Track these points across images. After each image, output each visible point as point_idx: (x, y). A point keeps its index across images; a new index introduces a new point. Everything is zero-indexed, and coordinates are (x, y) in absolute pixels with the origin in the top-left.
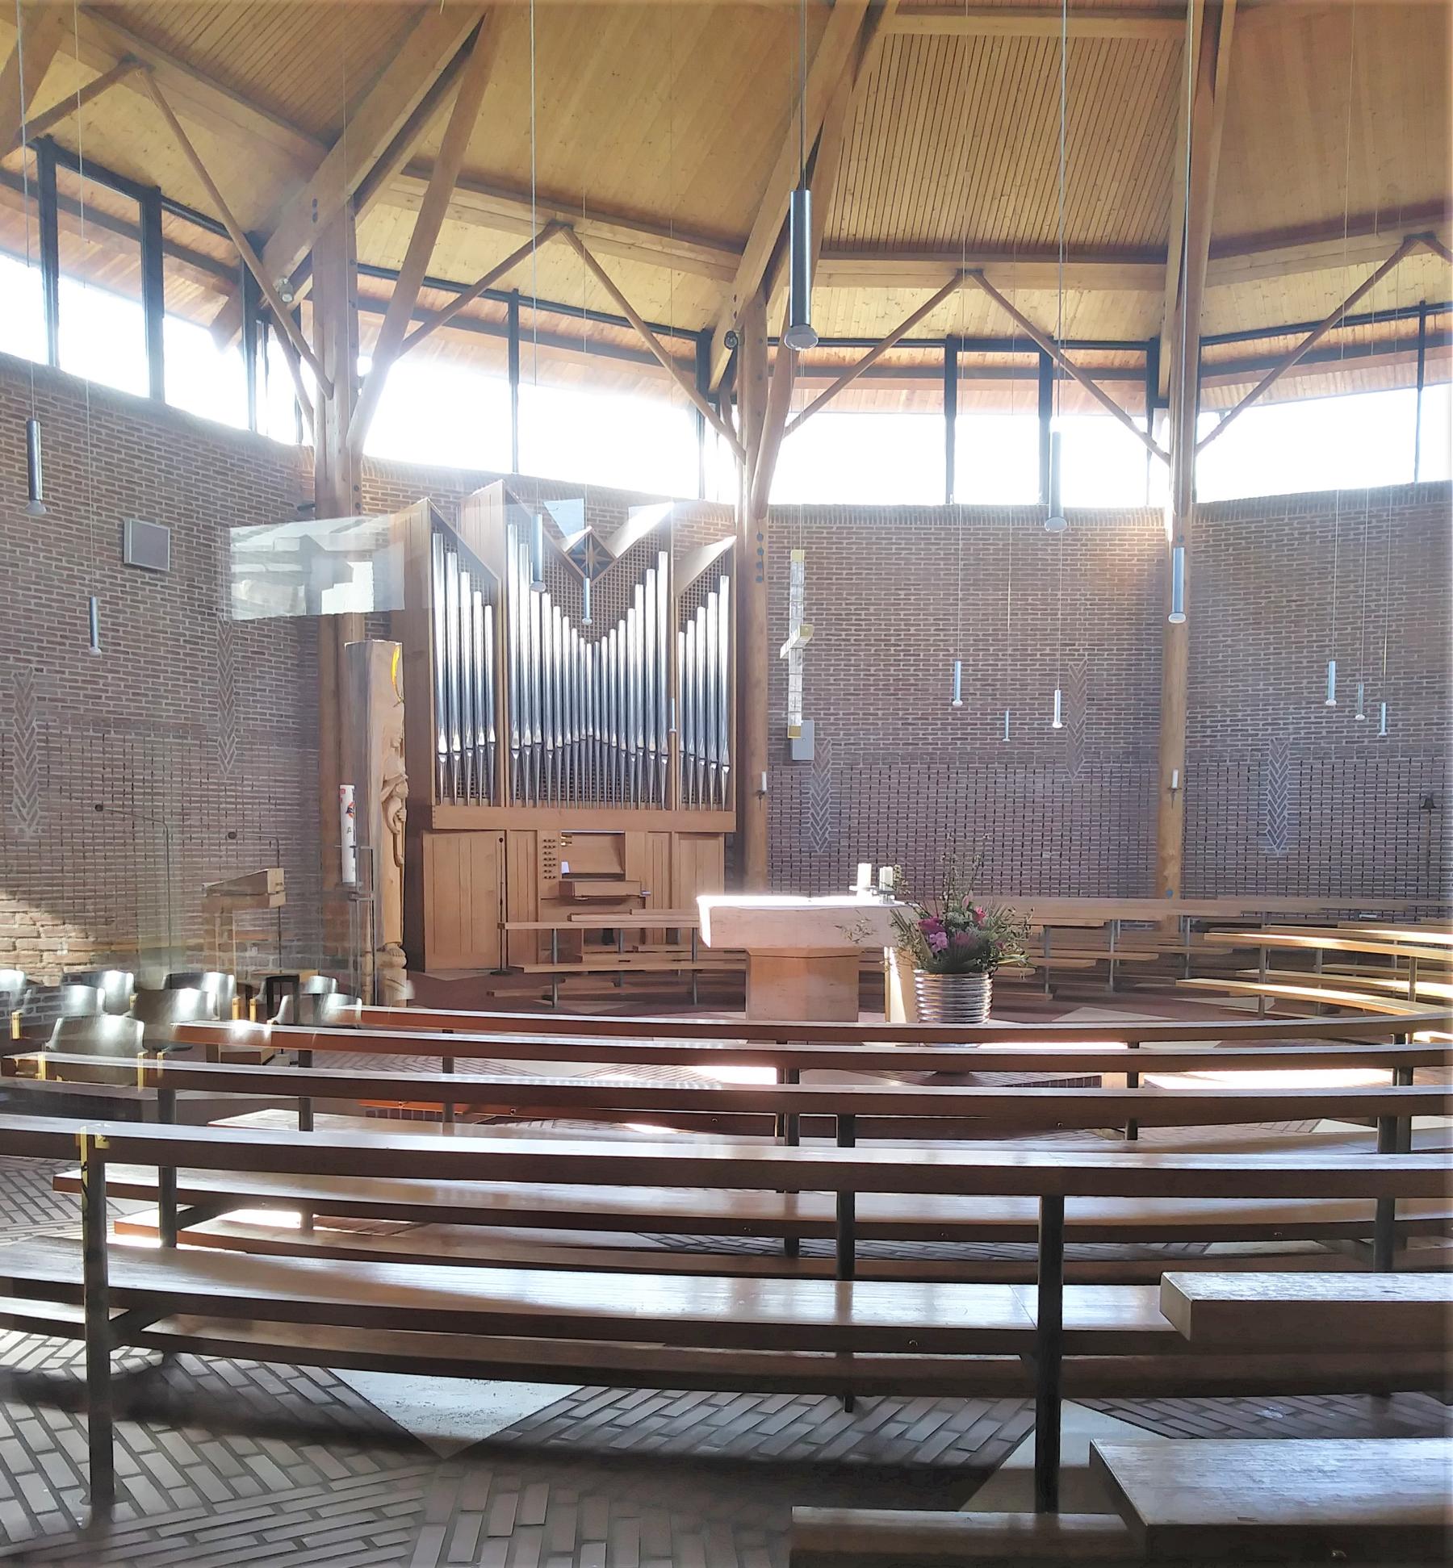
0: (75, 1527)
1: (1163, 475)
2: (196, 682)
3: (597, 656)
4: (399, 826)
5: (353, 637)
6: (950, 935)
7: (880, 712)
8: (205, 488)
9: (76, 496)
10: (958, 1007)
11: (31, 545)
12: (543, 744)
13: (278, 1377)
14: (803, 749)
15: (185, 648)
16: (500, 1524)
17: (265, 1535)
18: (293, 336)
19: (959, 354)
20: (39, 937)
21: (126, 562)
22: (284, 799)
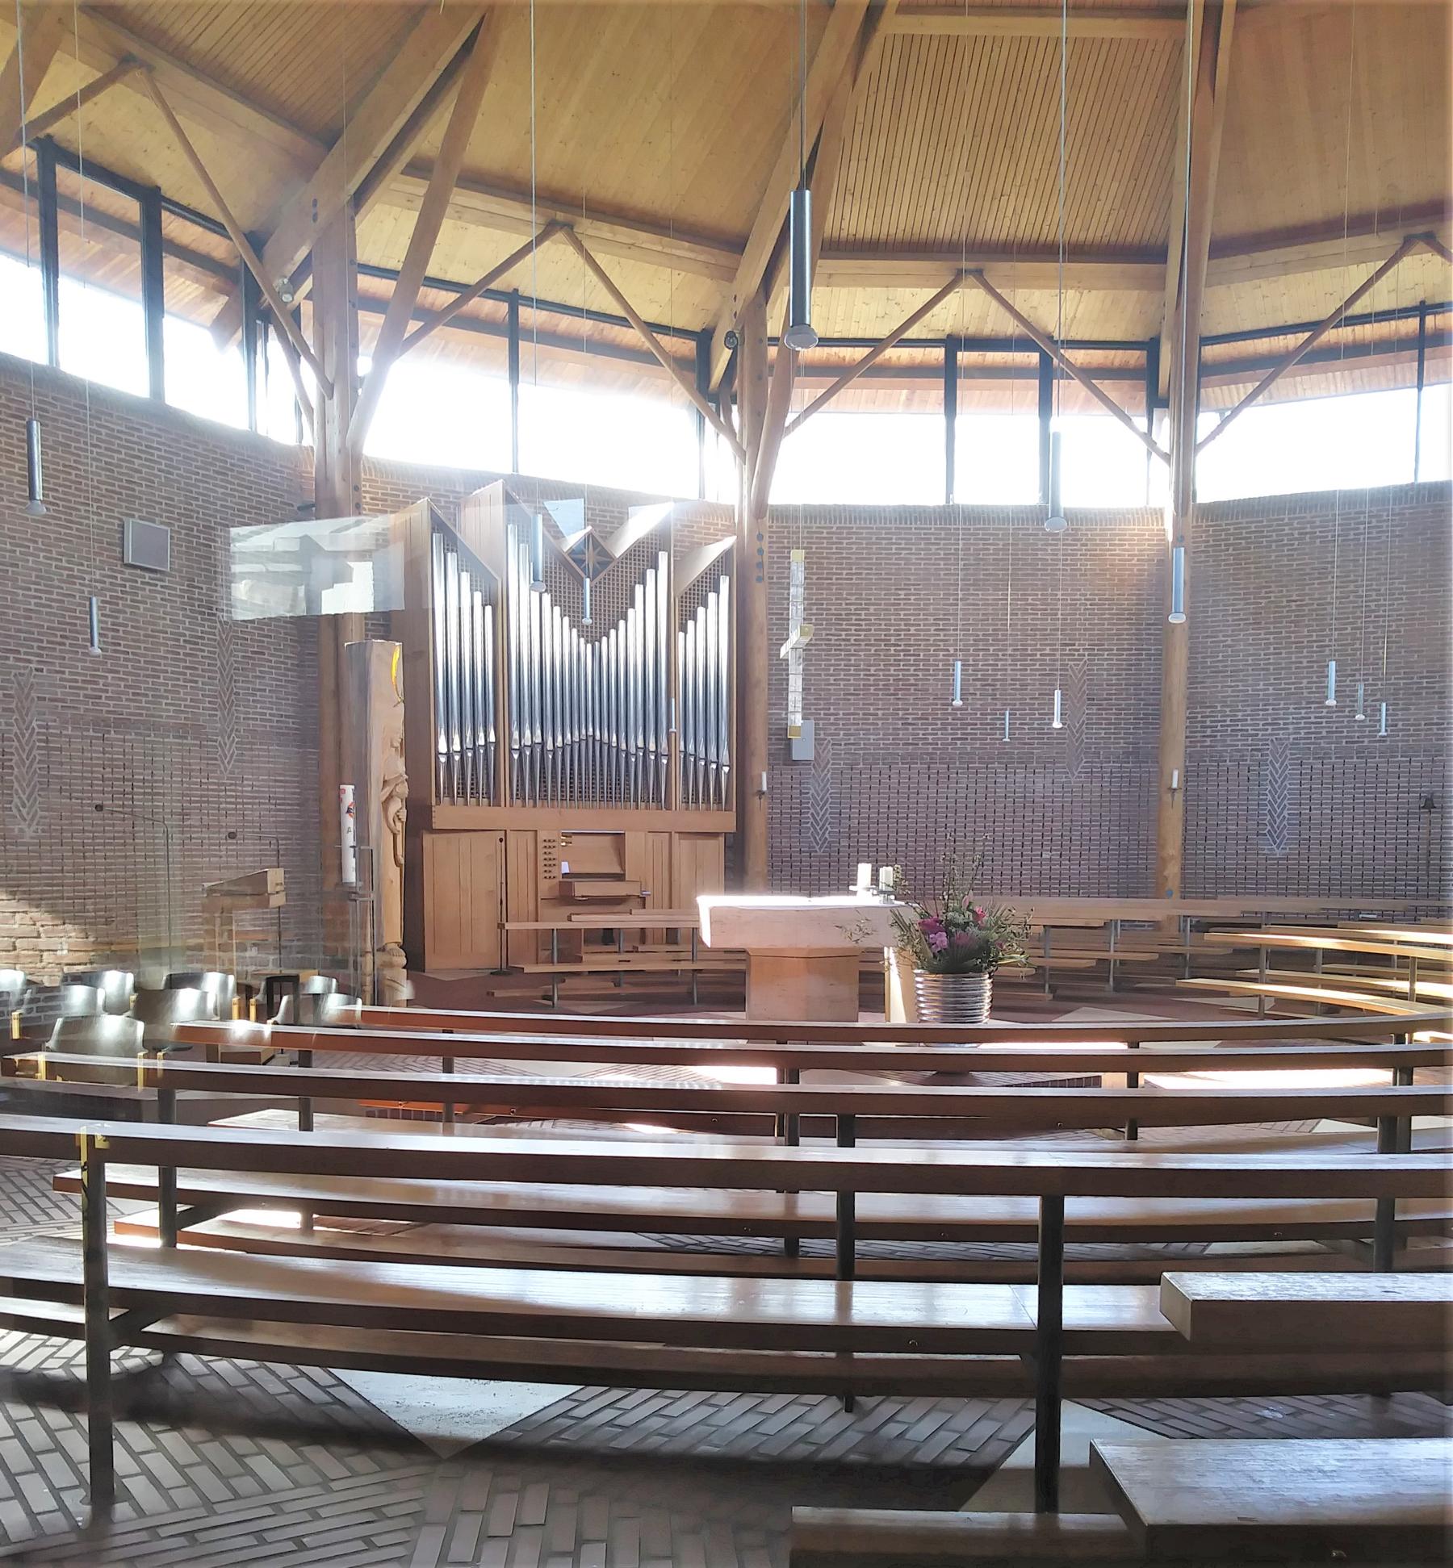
0: (75, 1527)
1: (1163, 475)
2: (196, 682)
3: (597, 656)
4: (399, 826)
5: (353, 637)
6: (950, 935)
7: (880, 712)
8: (205, 488)
9: (76, 496)
10: (958, 1007)
11: (31, 545)
12: (543, 744)
13: (278, 1377)
14: (803, 749)
15: (185, 648)
16: (500, 1524)
17: (265, 1535)
18: (293, 336)
19: (959, 354)
20: (39, 937)
21: (126, 562)
22: (284, 799)
